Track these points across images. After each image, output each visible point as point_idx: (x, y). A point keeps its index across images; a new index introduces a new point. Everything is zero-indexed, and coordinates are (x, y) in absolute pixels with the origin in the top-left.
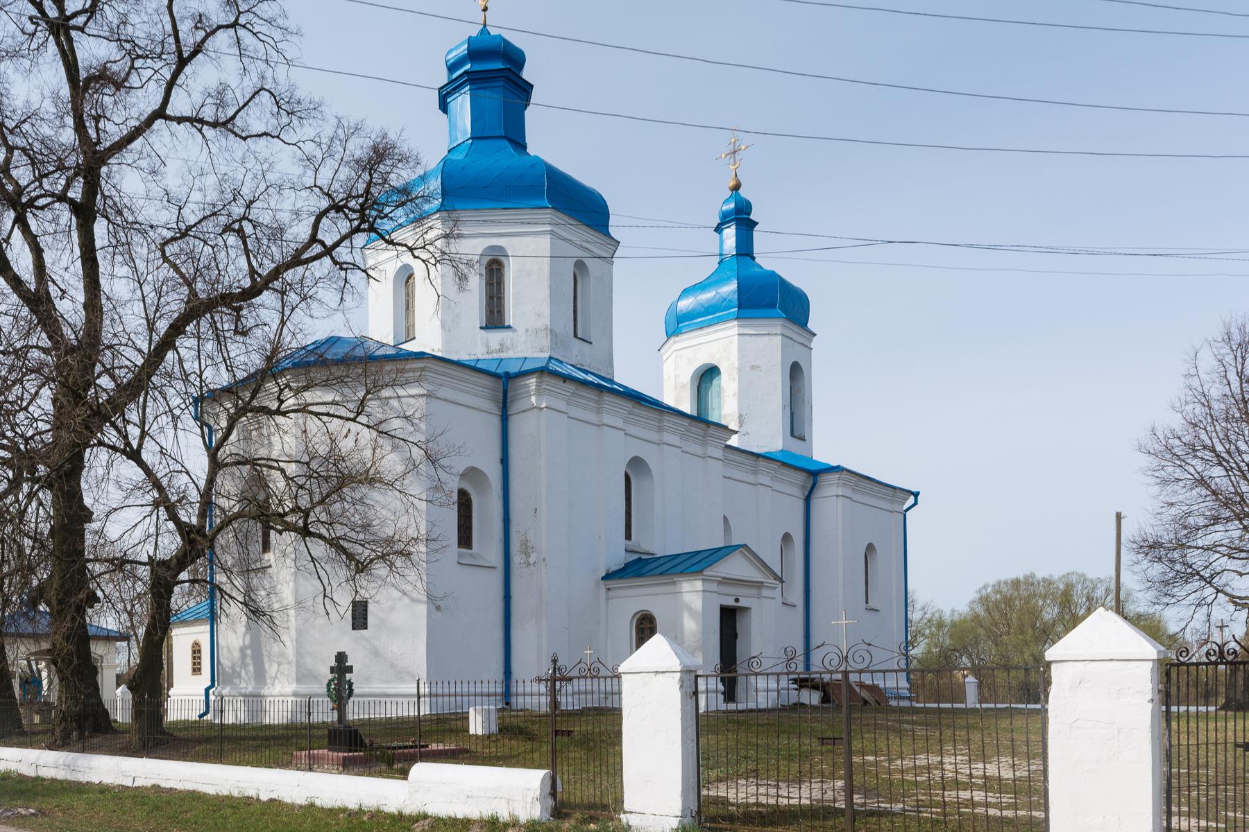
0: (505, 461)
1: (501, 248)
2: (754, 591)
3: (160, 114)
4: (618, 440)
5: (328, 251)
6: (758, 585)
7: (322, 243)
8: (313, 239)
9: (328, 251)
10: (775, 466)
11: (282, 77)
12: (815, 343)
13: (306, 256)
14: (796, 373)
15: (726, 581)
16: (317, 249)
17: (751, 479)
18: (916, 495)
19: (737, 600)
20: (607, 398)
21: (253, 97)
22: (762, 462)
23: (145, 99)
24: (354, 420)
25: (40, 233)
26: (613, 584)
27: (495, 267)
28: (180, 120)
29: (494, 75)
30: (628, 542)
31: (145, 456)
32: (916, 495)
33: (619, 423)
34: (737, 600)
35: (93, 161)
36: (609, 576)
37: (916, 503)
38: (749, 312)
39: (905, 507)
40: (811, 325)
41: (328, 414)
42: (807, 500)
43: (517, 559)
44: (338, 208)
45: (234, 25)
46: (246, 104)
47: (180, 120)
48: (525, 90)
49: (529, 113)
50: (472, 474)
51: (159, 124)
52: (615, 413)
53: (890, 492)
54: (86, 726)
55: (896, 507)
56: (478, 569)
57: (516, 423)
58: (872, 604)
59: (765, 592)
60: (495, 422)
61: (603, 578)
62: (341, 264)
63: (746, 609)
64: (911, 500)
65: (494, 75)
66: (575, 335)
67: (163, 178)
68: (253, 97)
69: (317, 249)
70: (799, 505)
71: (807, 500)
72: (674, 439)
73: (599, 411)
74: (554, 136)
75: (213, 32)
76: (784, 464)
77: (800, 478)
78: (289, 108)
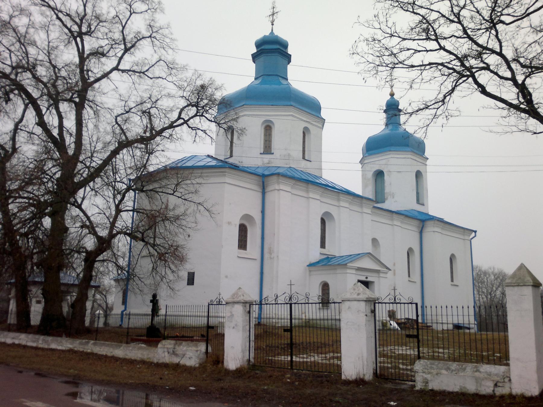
0: (263, 212)
1: (270, 121)
2: (375, 275)
3: (116, 68)
4: (317, 205)
5: (186, 122)
6: (378, 272)
7: (183, 119)
8: (179, 118)
9: (186, 122)
10: (403, 217)
11: (169, 56)
12: (428, 162)
13: (175, 124)
14: (419, 175)
15: (359, 269)
16: (181, 121)
17: (390, 223)
18: (475, 232)
19: (367, 278)
20: (310, 186)
21: (156, 63)
22: (394, 215)
23: (109, 63)
24: (173, 194)
25: (172, 72)
26: (313, 268)
27: (268, 128)
28: (123, 71)
29: (272, 52)
30: (323, 250)
31: (83, 207)
32: (475, 232)
33: (318, 197)
34: (367, 278)
35: (86, 85)
36: (311, 265)
37: (475, 236)
38: (371, 152)
39: (471, 237)
40: (427, 154)
41: (162, 192)
42: (421, 233)
43: (266, 256)
44: (190, 105)
45: (150, 37)
46: (153, 66)
47: (123, 71)
48: (288, 58)
49: (289, 67)
50: (247, 217)
51: (115, 72)
52: (314, 194)
53: (462, 230)
54: (52, 325)
55: (466, 238)
56: (248, 260)
57: (268, 196)
58: (455, 282)
59: (381, 275)
60: (260, 195)
61: (308, 266)
62: (192, 128)
63: (373, 282)
64: (473, 234)
65: (272, 52)
66: (304, 158)
67: (113, 94)
68: (156, 63)
69: (181, 121)
70: (417, 235)
71: (421, 233)
72: (347, 205)
73: (307, 192)
74: (299, 77)
75: (141, 39)
76: (407, 216)
77: (416, 223)
78: (171, 67)
